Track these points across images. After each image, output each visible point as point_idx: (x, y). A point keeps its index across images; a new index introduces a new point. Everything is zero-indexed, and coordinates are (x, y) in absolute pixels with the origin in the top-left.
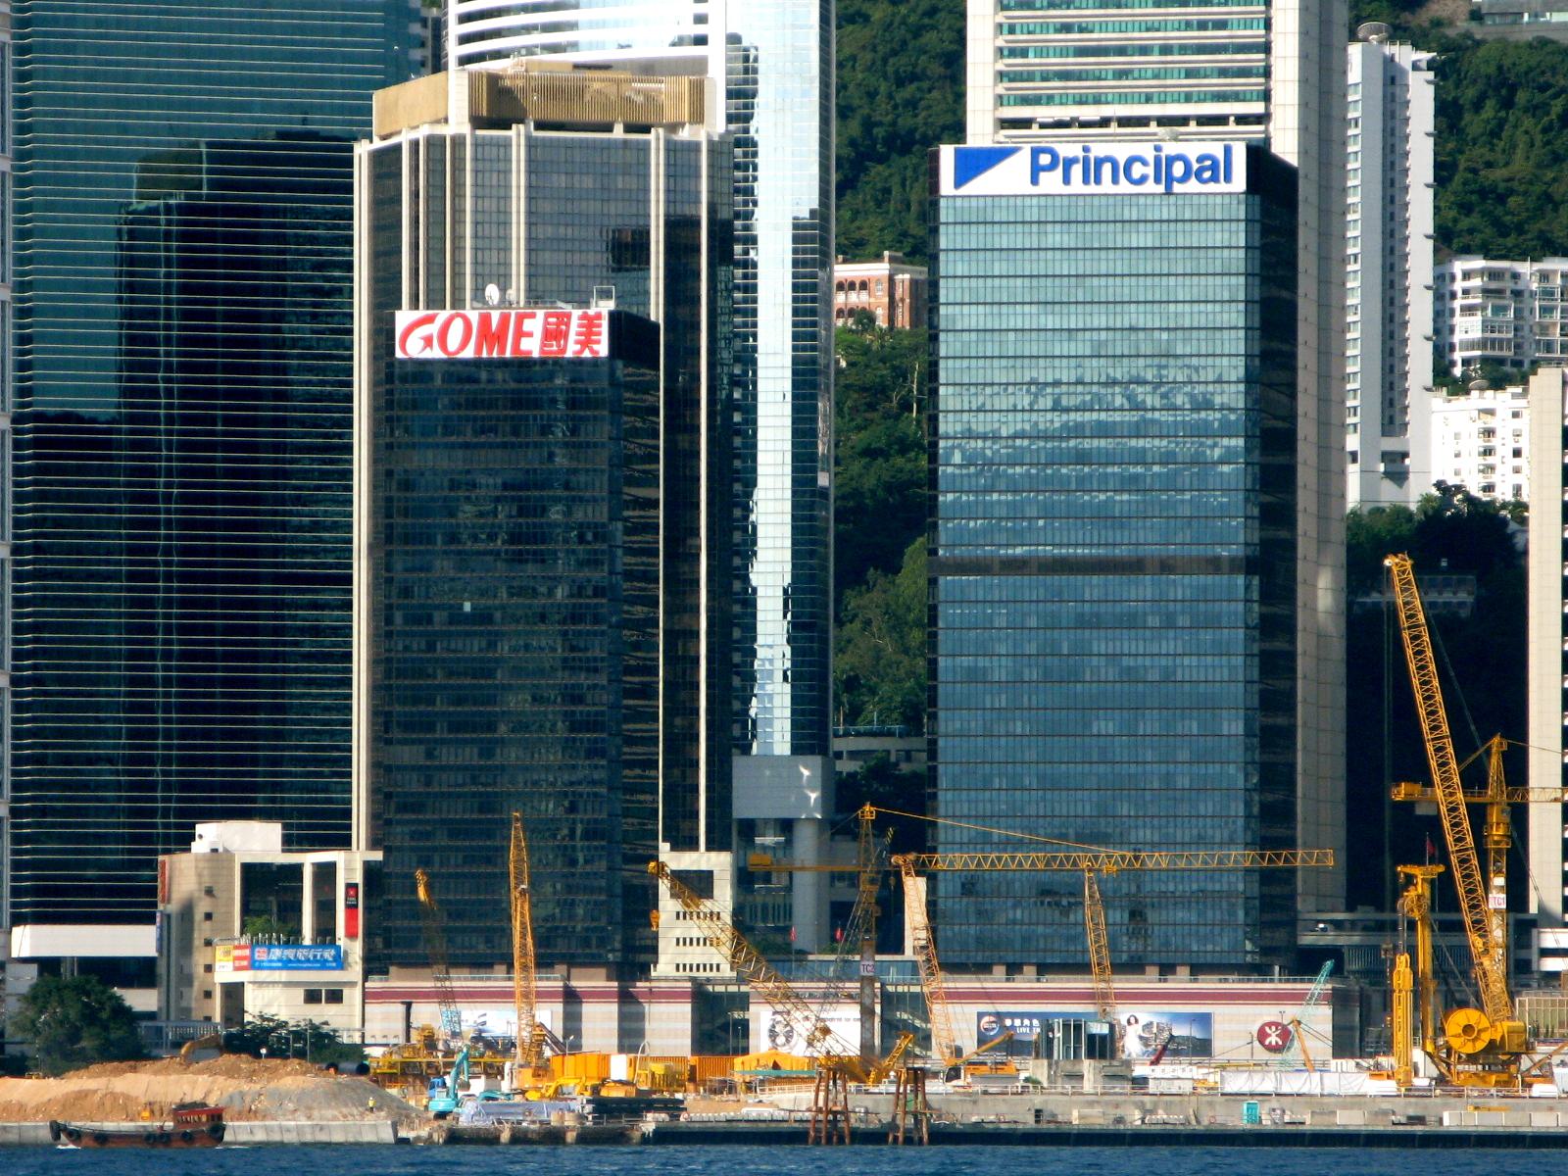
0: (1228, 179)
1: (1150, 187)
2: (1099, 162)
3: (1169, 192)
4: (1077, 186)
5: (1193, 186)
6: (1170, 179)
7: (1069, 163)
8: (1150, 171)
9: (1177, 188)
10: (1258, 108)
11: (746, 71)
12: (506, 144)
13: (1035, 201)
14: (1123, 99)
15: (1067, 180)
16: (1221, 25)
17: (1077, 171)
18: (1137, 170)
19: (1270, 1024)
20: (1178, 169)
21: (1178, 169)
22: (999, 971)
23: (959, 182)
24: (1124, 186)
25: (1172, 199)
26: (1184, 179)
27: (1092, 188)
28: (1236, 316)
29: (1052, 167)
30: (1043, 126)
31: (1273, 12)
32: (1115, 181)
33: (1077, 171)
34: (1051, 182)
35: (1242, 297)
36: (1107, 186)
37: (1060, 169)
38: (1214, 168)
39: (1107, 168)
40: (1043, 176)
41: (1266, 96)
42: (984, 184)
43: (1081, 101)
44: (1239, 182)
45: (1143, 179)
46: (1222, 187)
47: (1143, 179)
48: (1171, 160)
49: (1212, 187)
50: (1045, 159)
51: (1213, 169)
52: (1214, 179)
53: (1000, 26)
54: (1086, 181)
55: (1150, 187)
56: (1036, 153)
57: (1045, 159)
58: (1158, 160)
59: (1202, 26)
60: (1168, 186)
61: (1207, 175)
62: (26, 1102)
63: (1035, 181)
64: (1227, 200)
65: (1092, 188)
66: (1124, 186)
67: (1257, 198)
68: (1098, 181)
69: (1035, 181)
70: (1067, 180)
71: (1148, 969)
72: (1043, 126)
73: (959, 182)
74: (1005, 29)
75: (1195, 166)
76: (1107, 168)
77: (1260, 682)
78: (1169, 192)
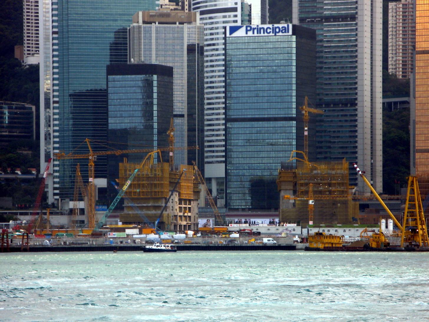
2: (260, 29)
3: (275, 35)
4: (256, 34)
5: (280, 34)
9: (277, 34)
12: (151, 27)
15: (253, 33)
17: (256, 31)
21: (277, 30)
26: (279, 32)
29: (250, 30)
33: (256, 31)
34: (250, 33)
36: (262, 34)
38: (285, 30)
39: (262, 31)
42: (235, 34)
48: (276, 28)
51: (286, 30)
52: (285, 32)
63: (247, 33)
65: (253, 35)
66: (266, 34)
69: (247, 33)
70: (253, 33)
76: (262, 31)
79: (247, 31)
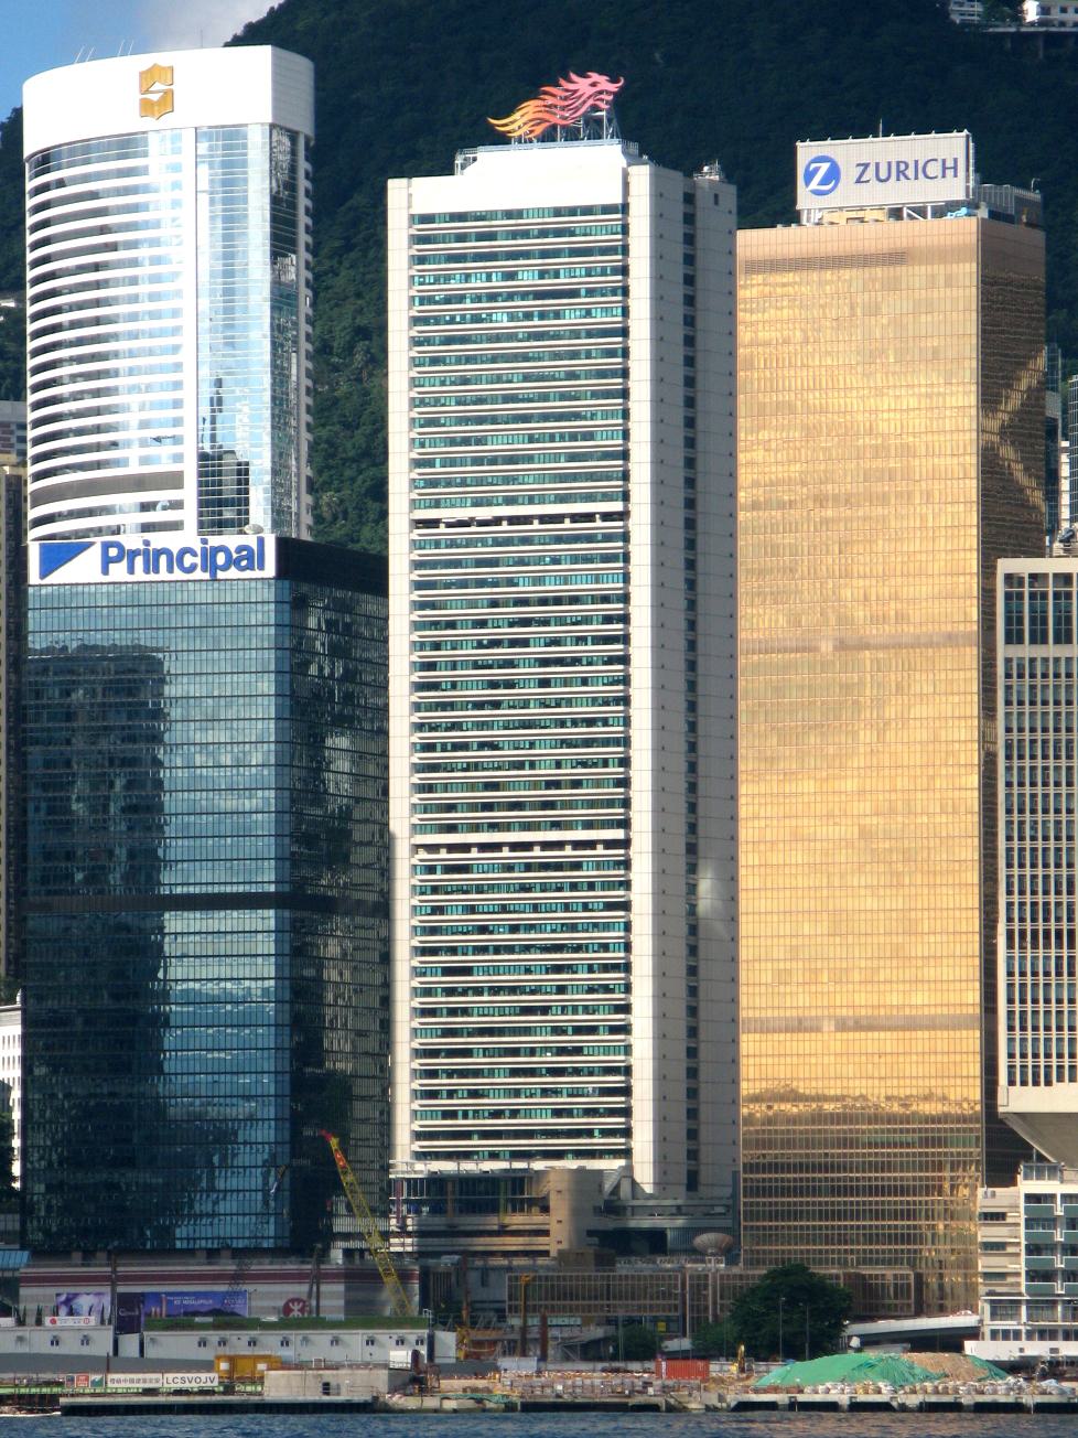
0: (261, 567)
1: (199, 574)
3: (214, 579)
4: (140, 575)
5: (233, 573)
6: (214, 568)
7: (133, 554)
8: (198, 560)
9: (221, 575)
10: (617, 506)
11: (239, 482)
13: (105, 588)
14: (510, 501)
15: (131, 570)
16: (589, 436)
17: (139, 561)
18: (188, 560)
19: (293, 1301)
20: (221, 559)
21: (221, 559)
22: (77, 1257)
23: (44, 573)
24: (178, 575)
25: (216, 585)
26: (225, 568)
27: (152, 577)
28: (267, 685)
29: (118, 559)
30: (449, 525)
31: (631, 425)
32: (170, 570)
33: (139, 561)
34: (119, 572)
35: (272, 668)
36: (163, 575)
37: (125, 562)
38: (250, 557)
39: (163, 559)
40: (112, 566)
41: (626, 497)
42: (67, 574)
43: (477, 503)
44: (270, 569)
45: (192, 568)
46: (257, 574)
47: (192, 568)
49: (248, 574)
50: (113, 552)
52: (250, 567)
53: (413, 440)
54: (147, 571)
55: (199, 574)
56: (106, 546)
57: (113, 552)
58: (204, 551)
59: (573, 437)
60: (213, 574)
61: (244, 563)
62: (7, 1413)
63: (105, 571)
64: (259, 585)
65: (152, 577)
66: (178, 575)
67: (287, 583)
68: (157, 571)
69: (105, 571)
70: (131, 570)
71: (99, 1254)
72: (449, 525)
73: (44, 573)
74: (417, 442)
75: (235, 556)
76: (163, 559)
77: (291, 1002)
78: (214, 579)
79: (107, 562)
